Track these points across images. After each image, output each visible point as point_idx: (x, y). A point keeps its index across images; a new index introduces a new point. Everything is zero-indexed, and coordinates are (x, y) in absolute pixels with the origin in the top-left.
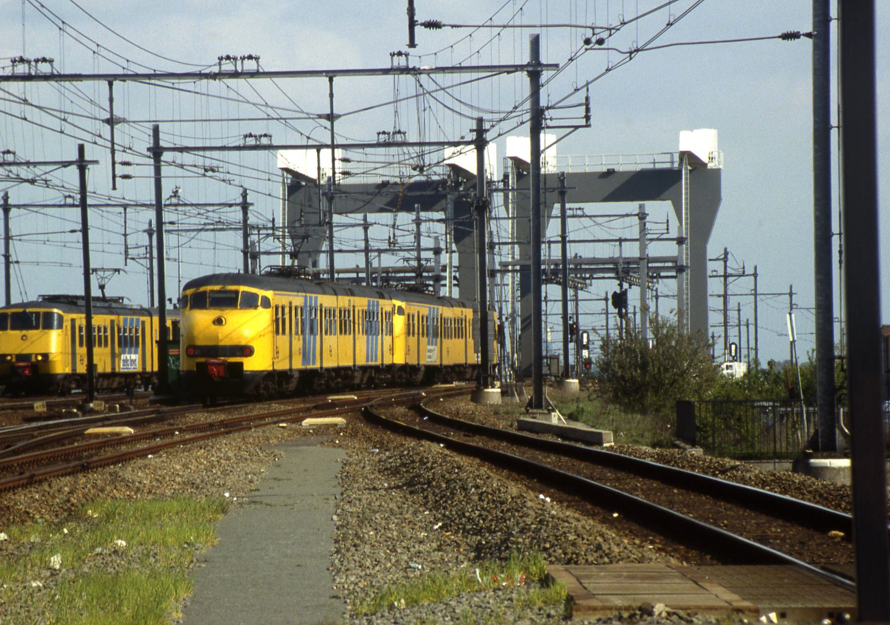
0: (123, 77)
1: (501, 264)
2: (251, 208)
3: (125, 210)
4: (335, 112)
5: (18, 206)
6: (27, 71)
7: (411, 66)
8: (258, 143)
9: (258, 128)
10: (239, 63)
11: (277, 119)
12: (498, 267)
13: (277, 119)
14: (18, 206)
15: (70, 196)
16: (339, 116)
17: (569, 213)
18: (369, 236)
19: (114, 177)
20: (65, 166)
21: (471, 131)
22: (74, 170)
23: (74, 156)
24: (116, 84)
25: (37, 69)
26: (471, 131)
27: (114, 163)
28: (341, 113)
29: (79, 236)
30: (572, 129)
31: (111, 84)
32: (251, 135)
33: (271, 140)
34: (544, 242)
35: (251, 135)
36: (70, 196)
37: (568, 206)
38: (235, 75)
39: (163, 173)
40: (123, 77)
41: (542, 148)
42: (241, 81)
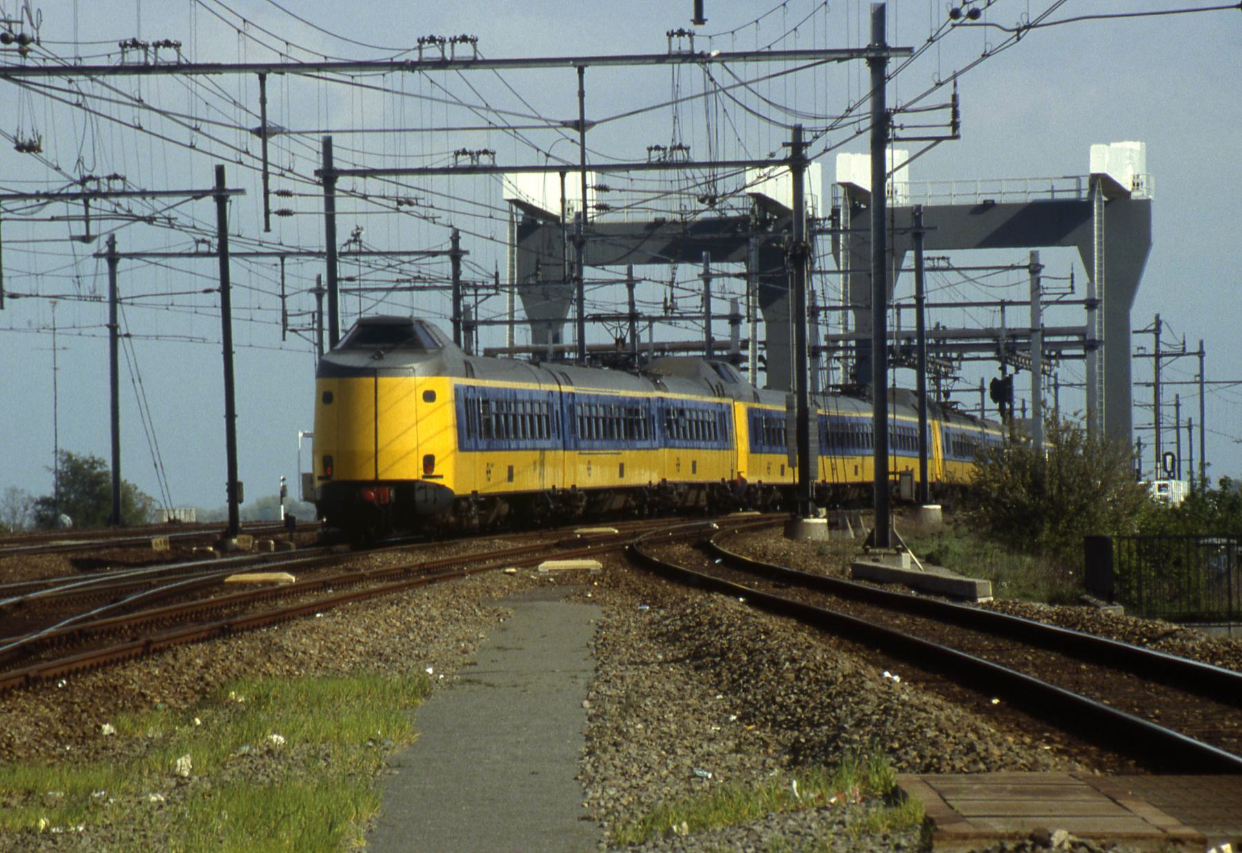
0: (281, 68)
1: (827, 338)
2: (464, 257)
3: (282, 260)
4: (586, 118)
5: (131, 256)
6: (142, 60)
7: (697, 51)
8: (475, 163)
9: (475, 142)
10: (448, 46)
11: (503, 128)
12: (823, 343)
13: (503, 128)
14: (131, 256)
15: (203, 241)
16: (593, 124)
17: (927, 264)
18: (636, 297)
19: (267, 213)
20: (197, 198)
21: (785, 145)
22: (209, 203)
23: (211, 183)
24: (271, 77)
25: (156, 57)
26: (785, 145)
27: (267, 193)
28: (595, 120)
29: (217, 297)
30: (931, 142)
31: (262, 79)
32: (464, 152)
33: (493, 159)
34: (891, 307)
35: (464, 152)
36: (203, 241)
37: (926, 254)
38: (442, 64)
39: (338, 208)
40: (281, 68)
41: (888, 169)
42: (451, 74)
